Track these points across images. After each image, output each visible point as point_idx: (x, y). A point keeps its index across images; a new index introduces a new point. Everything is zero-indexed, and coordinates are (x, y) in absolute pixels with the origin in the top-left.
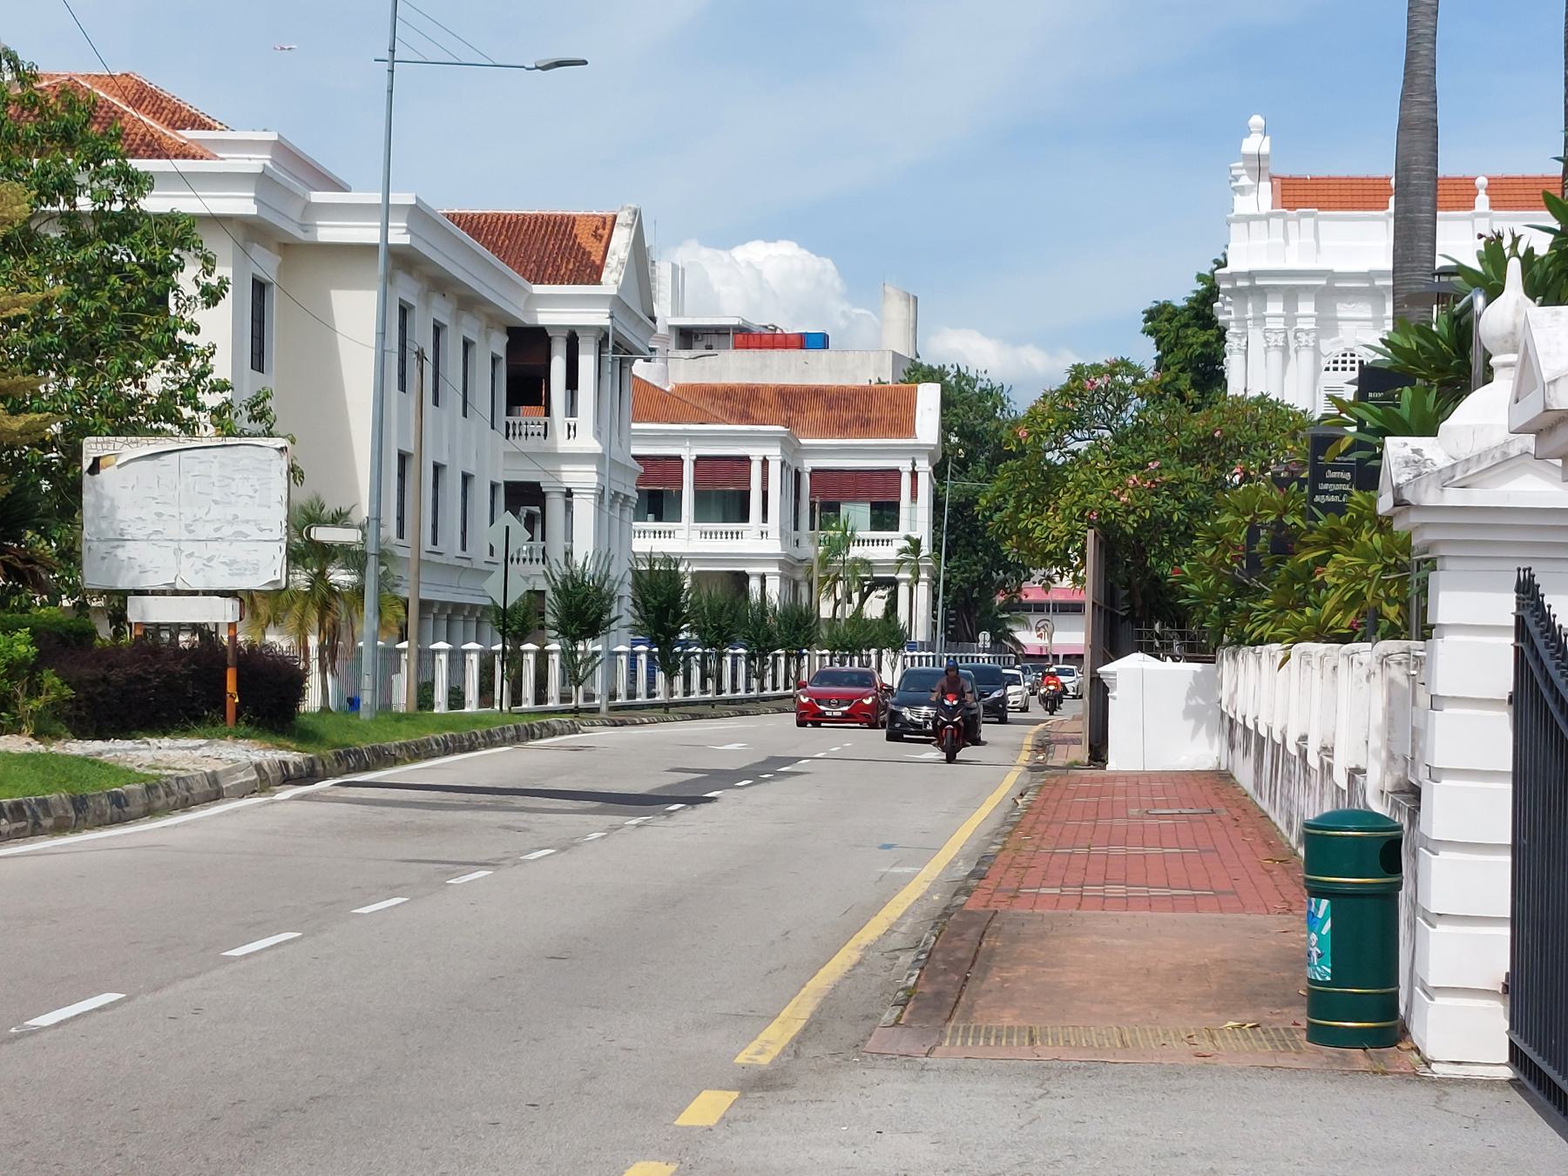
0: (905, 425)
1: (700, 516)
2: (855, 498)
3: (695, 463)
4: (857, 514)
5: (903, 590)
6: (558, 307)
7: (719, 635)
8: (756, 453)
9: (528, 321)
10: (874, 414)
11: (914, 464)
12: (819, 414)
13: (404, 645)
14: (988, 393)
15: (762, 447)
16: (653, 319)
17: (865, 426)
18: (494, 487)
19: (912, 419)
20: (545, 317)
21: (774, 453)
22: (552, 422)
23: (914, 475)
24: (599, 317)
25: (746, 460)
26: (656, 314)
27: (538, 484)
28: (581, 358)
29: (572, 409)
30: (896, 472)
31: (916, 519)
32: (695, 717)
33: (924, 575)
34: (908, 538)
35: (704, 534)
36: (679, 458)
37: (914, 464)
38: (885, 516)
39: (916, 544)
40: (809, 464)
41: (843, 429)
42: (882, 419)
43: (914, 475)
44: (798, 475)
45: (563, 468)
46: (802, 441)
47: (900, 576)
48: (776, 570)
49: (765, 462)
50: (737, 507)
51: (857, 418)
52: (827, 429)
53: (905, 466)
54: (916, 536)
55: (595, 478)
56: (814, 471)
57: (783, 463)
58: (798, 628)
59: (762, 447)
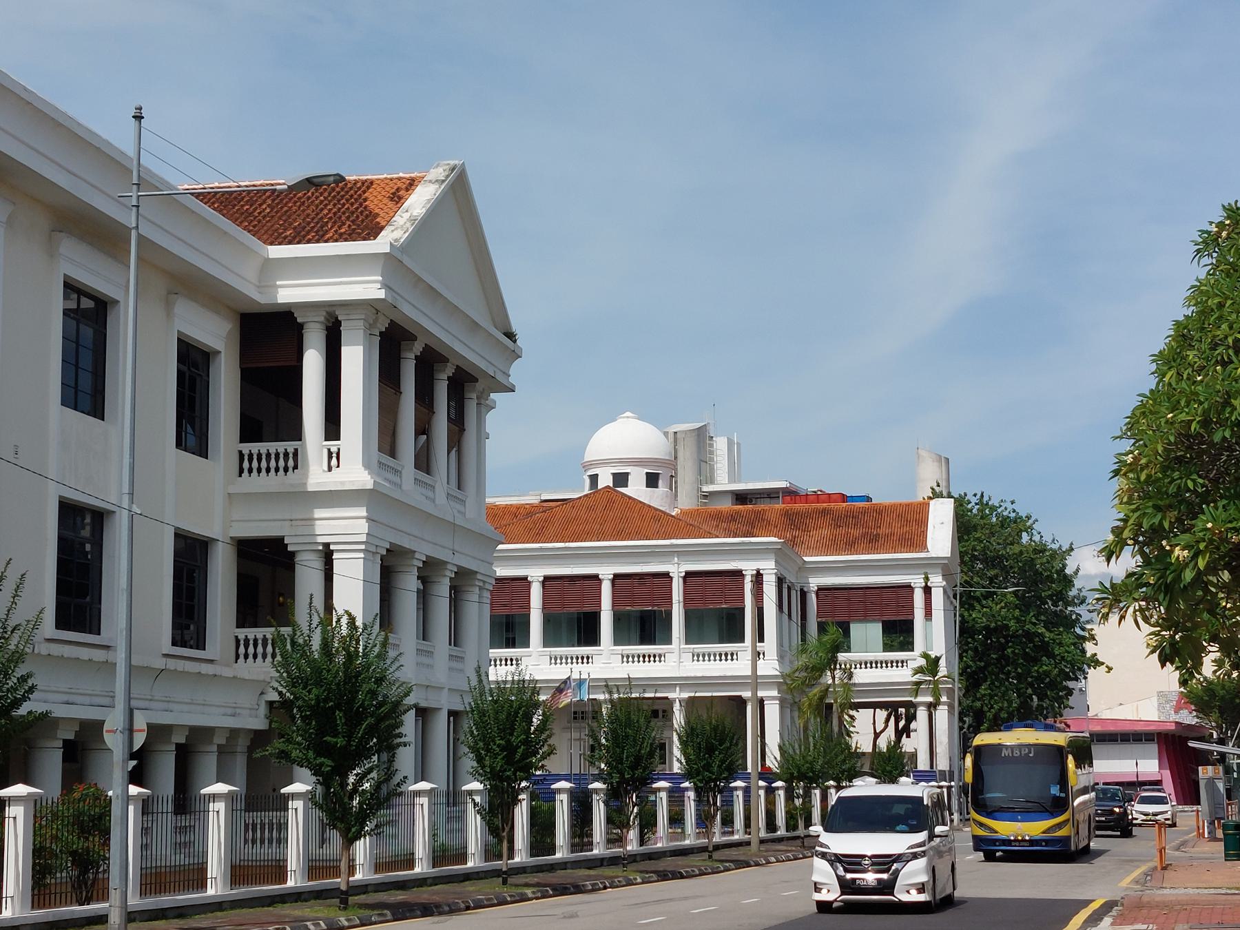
0: (917, 539)
1: (693, 635)
2: (865, 618)
3: (685, 578)
4: (867, 636)
5: (922, 714)
6: (315, 277)
7: (509, 760)
8: (749, 567)
9: (261, 298)
10: (884, 530)
11: (927, 579)
12: (825, 532)
13: (424, 785)
14: (1004, 522)
15: (757, 561)
16: (511, 336)
17: (873, 542)
18: (191, 554)
19: (924, 534)
20: (289, 293)
21: (769, 567)
22: (304, 447)
23: (927, 590)
24: (368, 288)
25: (739, 574)
26: (516, 327)
27: (281, 539)
28: (345, 351)
29: (332, 427)
30: (909, 588)
31: (934, 634)
32: (664, 876)
33: (944, 699)
34: (925, 656)
35: (697, 656)
36: (666, 575)
37: (927, 579)
38: (899, 633)
39: (932, 664)
40: (815, 582)
41: (851, 545)
42: (892, 534)
43: (927, 590)
44: (804, 594)
45: (319, 513)
46: (806, 559)
47: (920, 699)
48: (775, 693)
49: (758, 577)
50: (730, 627)
51: (864, 535)
52: (833, 546)
53: (917, 581)
54: (933, 654)
55: (362, 527)
56: (821, 590)
57: (780, 581)
58: (710, 750)
59: (757, 561)
